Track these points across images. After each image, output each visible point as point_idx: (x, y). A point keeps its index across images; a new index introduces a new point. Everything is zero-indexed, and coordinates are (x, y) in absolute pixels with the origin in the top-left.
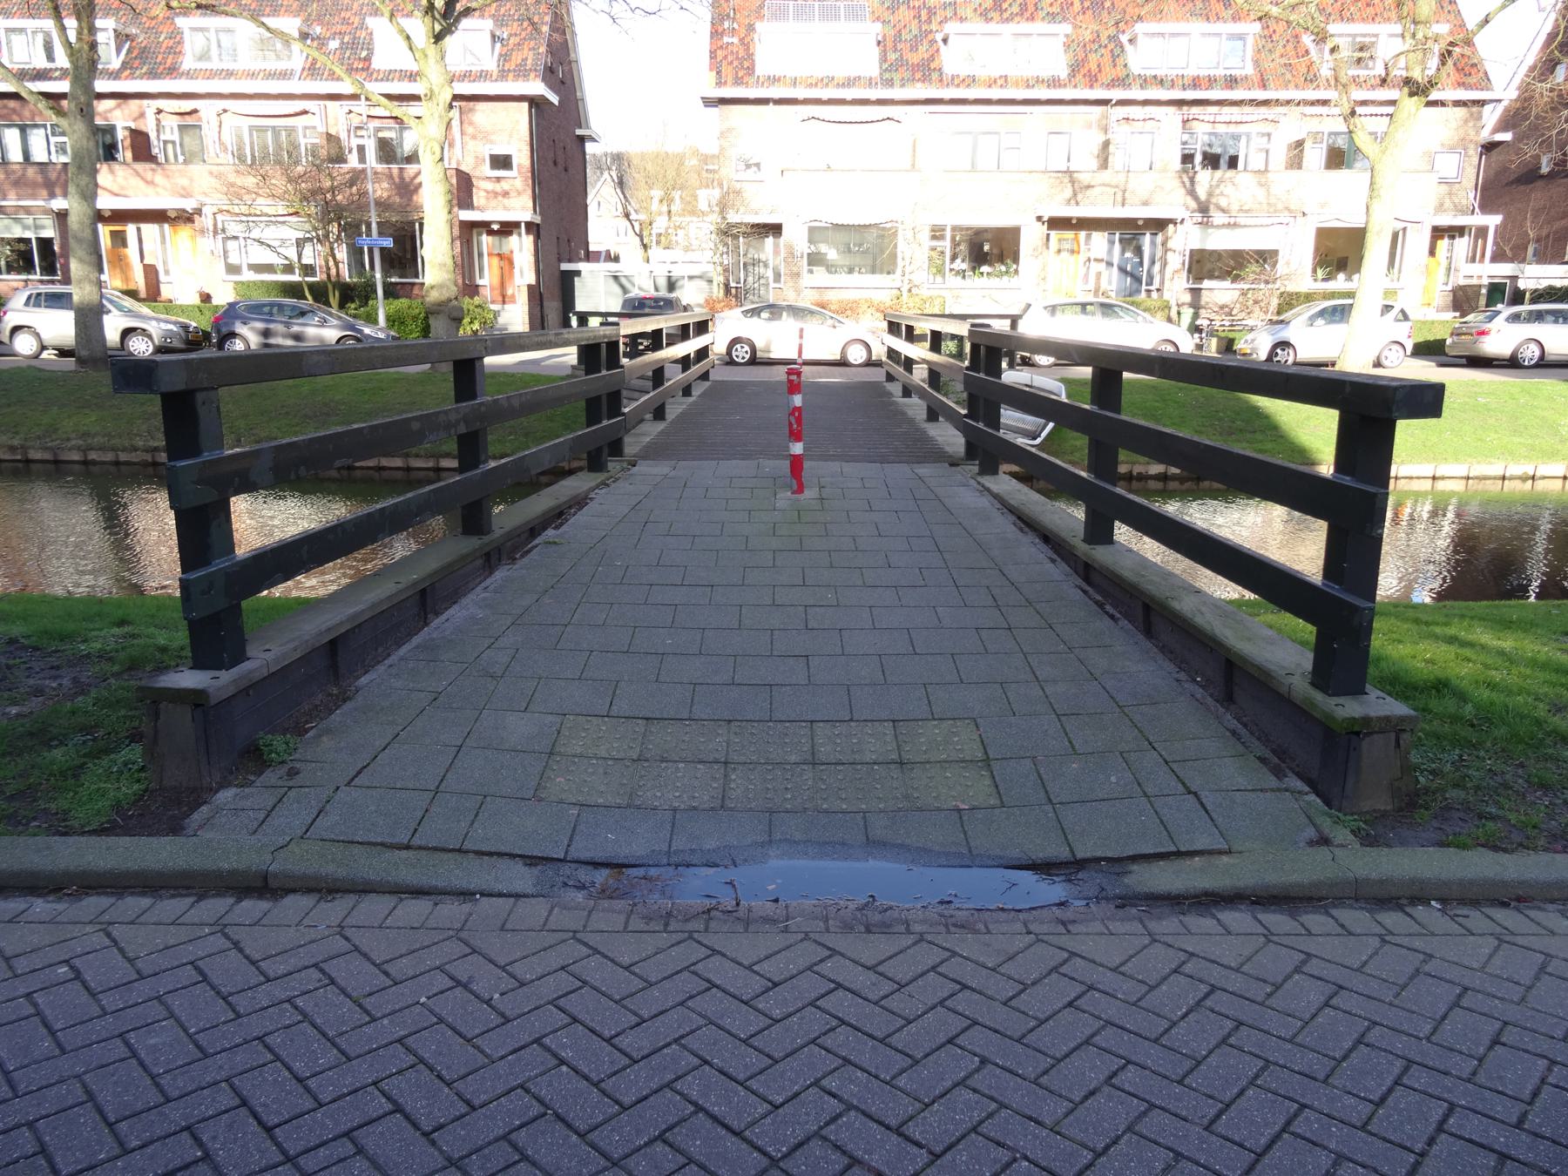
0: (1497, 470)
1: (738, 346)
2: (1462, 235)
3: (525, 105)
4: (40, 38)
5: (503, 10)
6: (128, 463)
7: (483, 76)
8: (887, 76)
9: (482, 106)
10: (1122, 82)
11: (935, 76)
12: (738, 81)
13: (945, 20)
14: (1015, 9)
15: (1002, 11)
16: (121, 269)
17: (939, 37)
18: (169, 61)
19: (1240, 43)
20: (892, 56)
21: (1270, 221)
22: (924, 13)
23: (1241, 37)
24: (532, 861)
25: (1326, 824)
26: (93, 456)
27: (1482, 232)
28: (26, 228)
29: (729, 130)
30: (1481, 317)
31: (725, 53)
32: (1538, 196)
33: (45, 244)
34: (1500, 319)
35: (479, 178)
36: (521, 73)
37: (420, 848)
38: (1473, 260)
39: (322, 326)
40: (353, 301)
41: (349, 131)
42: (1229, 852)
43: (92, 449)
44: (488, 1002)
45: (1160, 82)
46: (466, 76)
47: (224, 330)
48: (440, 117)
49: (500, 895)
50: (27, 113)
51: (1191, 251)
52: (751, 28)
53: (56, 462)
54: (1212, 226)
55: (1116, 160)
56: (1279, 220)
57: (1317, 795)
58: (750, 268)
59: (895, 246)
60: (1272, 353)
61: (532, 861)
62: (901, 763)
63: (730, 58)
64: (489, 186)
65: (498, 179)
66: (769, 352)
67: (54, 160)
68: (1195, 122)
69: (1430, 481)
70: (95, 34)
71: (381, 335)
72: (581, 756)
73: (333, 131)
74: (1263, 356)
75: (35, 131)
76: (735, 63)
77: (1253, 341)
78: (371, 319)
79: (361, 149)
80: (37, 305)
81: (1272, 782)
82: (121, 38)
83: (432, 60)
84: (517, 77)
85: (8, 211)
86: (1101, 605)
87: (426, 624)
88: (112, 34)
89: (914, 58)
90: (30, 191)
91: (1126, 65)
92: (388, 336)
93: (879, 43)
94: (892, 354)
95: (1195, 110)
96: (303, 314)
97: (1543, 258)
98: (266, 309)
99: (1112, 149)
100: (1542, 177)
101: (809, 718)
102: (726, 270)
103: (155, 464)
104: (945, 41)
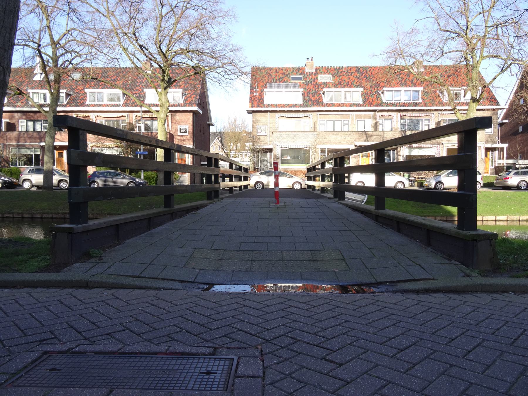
0: (517, 218)
1: (258, 184)
2: (495, 150)
3: (192, 113)
4: (42, 95)
5: (186, 87)
6: (56, 218)
7: (179, 105)
8: (305, 104)
9: (178, 114)
10: (381, 104)
11: (320, 104)
12: (258, 106)
13: (324, 87)
14: (345, 84)
15: (341, 85)
16: (60, 164)
17: (321, 92)
18: (82, 102)
19: (417, 93)
20: (307, 98)
21: (431, 146)
22: (317, 86)
23: (417, 91)
24: (182, 282)
25: (468, 272)
26: (45, 216)
27: (502, 149)
28: (32, 151)
29: (256, 120)
30: (505, 174)
31: (254, 98)
32: (519, 138)
33: (37, 156)
34: (512, 174)
35: (176, 135)
36: (191, 104)
37: (143, 277)
38: (500, 159)
39: (123, 179)
40: (133, 173)
41: (136, 122)
42: (433, 279)
43: (44, 213)
44: (164, 309)
45: (393, 105)
46: (173, 105)
47: (91, 180)
48: (165, 112)
49: (170, 289)
50: (36, 117)
51: (406, 156)
52: (262, 91)
53: (32, 218)
54: (413, 148)
55: (380, 128)
56: (435, 146)
57: (464, 265)
58: (262, 162)
59: (309, 153)
60: (436, 185)
61: (182, 282)
62: (314, 261)
63: (256, 99)
64: (179, 138)
65: (182, 136)
66: (269, 186)
67: (43, 130)
68: (405, 117)
69: (494, 222)
70: (59, 94)
71: (142, 182)
72: (201, 258)
73: (131, 122)
74: (433, 186)
75: (38, 122)
76: (258, 101)
77: (429, 182)
78: (139, 177)
79: (139, 127)
80: (32, 172)
81: (447, 262)
82: (68, 95)
83: (163, 95)
84: (189, 106)
85: (27, 146)
86: (382, 226)
87: (150, 230)
88: (65, 93)
89: (314, 99)
90: (34, 140)
91: (381, 100)
92: (144, 182)
93: (303, 94)
94: (309, 186)
95: (404, 113)
96: (117, 175)
97: (523, 158)
98: (105, 174)
99: (378, 124)
100: (520, 133)
101: (281, 250)
102: (254, 163)
103: (65, 218)
104: (323, 93)
